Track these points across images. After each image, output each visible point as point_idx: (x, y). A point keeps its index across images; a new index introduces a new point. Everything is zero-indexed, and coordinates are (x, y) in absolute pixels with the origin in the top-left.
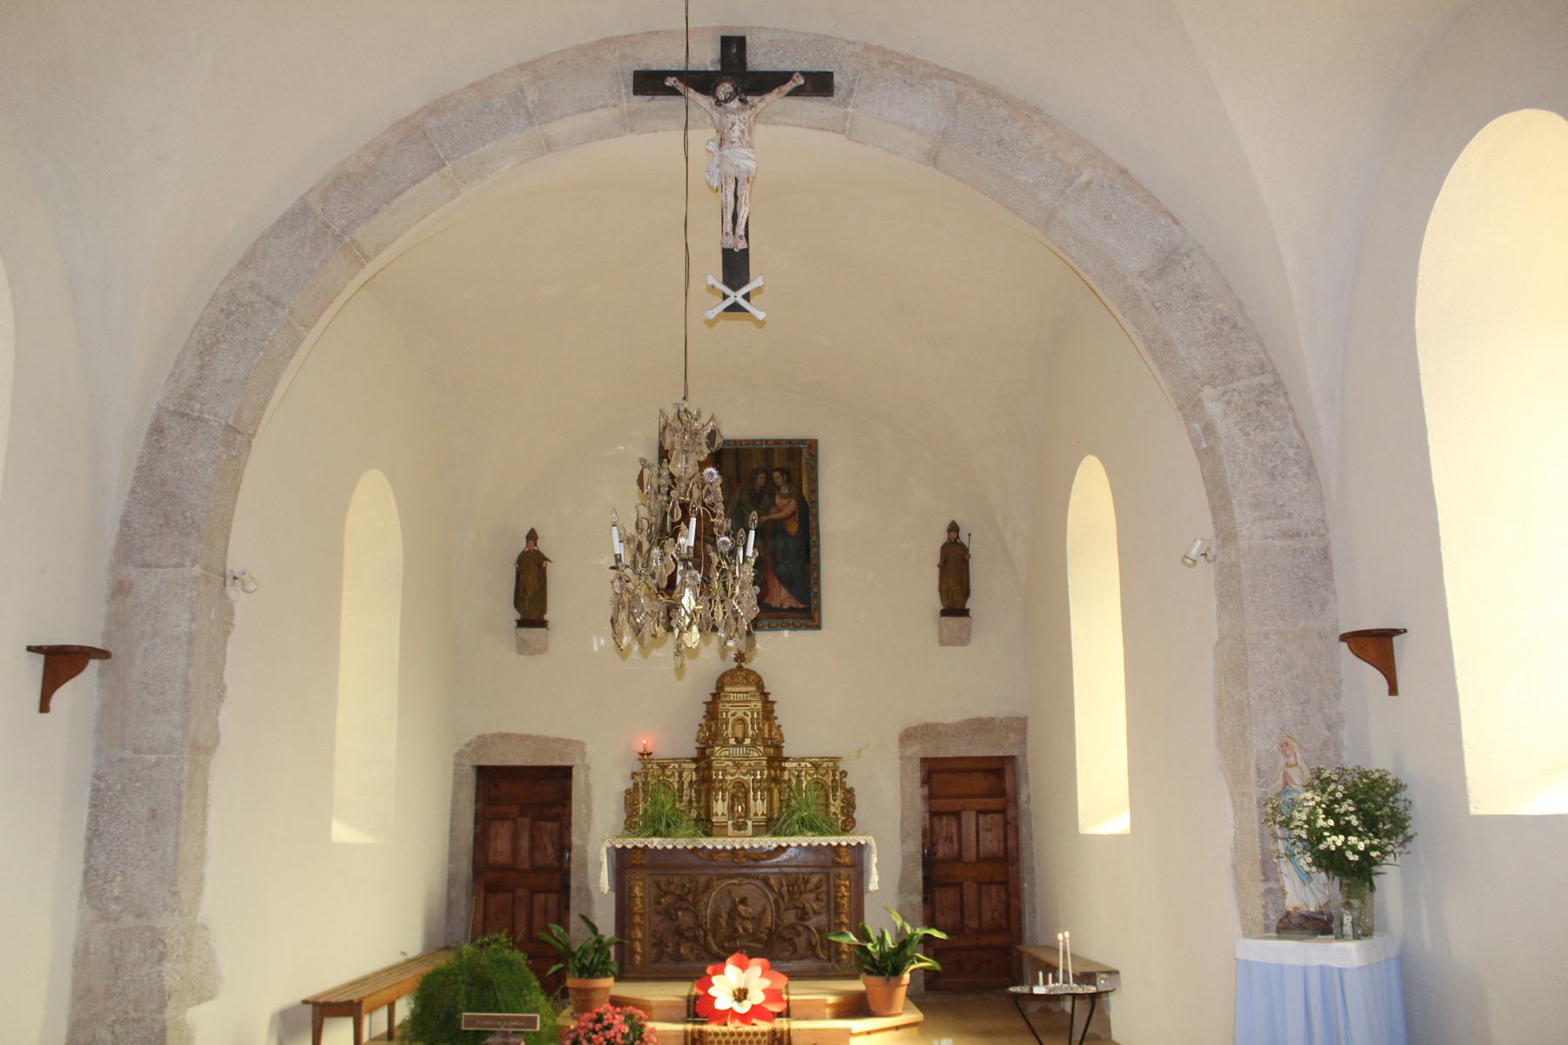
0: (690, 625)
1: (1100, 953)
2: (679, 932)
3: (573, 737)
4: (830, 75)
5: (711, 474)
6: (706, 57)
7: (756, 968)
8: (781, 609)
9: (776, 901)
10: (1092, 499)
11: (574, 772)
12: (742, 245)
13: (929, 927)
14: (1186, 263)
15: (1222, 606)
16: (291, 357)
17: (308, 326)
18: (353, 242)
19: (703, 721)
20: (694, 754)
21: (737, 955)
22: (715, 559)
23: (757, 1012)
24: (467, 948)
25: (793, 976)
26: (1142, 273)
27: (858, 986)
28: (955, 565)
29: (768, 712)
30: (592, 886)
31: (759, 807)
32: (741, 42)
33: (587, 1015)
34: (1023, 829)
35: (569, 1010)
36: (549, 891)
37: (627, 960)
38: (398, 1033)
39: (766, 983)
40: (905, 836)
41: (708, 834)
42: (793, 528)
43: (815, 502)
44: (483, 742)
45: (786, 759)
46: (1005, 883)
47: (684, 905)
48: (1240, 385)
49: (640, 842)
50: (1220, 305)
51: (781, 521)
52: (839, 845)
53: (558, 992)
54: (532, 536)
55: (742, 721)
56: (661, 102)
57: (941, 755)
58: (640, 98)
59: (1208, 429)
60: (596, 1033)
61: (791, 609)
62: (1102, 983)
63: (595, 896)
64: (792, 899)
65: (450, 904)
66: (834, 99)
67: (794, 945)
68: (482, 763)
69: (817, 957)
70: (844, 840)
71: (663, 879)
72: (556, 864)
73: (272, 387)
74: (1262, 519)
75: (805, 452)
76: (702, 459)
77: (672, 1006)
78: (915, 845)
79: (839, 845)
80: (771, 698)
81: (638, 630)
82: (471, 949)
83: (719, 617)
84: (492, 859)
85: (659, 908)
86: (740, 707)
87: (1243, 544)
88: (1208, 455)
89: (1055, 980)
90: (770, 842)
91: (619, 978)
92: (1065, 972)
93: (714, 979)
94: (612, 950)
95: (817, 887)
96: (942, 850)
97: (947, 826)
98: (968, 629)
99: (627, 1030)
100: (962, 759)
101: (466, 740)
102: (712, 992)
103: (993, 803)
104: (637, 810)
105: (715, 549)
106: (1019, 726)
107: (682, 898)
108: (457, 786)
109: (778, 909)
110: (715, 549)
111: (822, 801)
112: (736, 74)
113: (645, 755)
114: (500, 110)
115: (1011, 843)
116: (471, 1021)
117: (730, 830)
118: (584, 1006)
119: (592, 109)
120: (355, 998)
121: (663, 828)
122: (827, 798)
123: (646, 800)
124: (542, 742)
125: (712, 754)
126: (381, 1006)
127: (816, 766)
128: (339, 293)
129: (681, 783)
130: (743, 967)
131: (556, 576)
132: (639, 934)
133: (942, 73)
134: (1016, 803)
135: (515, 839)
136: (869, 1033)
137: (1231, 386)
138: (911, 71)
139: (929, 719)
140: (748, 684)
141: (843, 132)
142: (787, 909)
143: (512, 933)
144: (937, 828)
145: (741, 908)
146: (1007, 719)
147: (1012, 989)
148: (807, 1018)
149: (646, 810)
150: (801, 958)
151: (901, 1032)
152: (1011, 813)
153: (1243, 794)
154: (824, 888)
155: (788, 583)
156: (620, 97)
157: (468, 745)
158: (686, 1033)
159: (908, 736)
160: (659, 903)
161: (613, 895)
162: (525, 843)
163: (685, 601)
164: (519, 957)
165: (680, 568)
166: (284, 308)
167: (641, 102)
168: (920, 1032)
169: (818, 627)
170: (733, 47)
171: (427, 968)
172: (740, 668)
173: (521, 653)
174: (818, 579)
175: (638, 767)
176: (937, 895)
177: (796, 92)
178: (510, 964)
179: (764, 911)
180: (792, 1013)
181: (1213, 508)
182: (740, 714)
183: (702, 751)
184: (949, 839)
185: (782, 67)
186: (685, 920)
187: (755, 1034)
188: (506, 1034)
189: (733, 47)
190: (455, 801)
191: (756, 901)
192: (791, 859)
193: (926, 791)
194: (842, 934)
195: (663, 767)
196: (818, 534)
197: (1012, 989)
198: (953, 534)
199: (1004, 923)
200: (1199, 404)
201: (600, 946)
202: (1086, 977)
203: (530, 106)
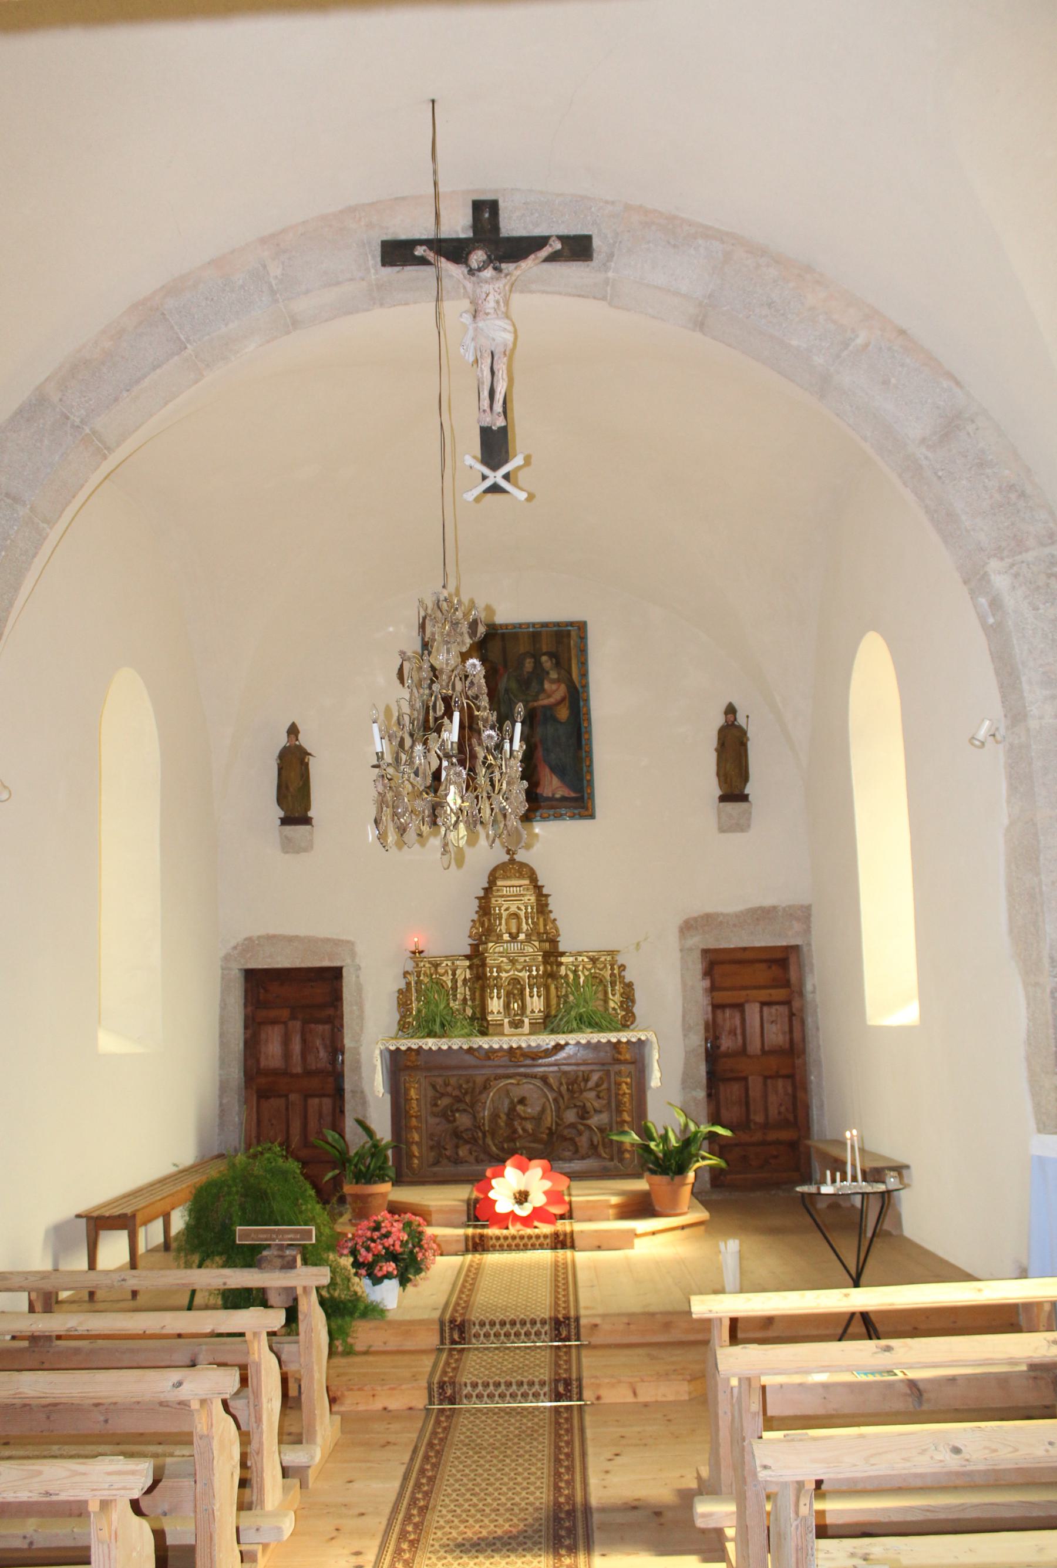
0: (456, 822)
1: (889, 1147)
2: (457, 1134)
3: (344, 938)
4: (588, 239)
5: (474, 665)
6: (458, 224)
7: (536, 1170)
8: (552, 799)
9: (555, 1100)
10: (874, 681)
12: (500, 422)
13: (713, 1124)
14: (970, 428)
15: (1013, 789)
16: (34, 556)
17: (51, 523)
18: (94, 432)
19: (475, 917)
21: (517, 1156)
22: (481, 753)
23: (539, 1214)
24: (241, 1158)
25: (573, 1176)
26: (923, 440)
27: (641, 1185)
28: (733, 747)
29: (542, 906)
31: (536, 1004)
33: (365, 1223)
34: (809, 1021)
35: (347, 1217)
36: (324, 1095)
37: (404, 1164)
38: (174, 1245)
39: (547, 1185)
40: (687, 1029)
41: (484, 1033)
42: (563, 714)
43: (586, 686)
44: (250, 945)
45: (563, 954)
46: (791, 1077)
47: (462, 1106)
48: (1030, 556)
49: (414, 1043)
50: (1007, 472)
51: (551, 708)
52: (619, 1042)
53: (334, 1200)
54: (293, 731)
55: (516, 916)
57: (724, 945)
58: (389, 270)
59: (996, 604)
60: (374, 1241)
61: (564, 799)
62: (892, 1182)
63: (370, 1098)
64: (573, 1098)
65: (223, 1111)
66: (594, 263)
67: (575, 1144)
69: (599, 1156)
70: (624, 1037)
71: (440, 1081)
72: (330, 1068)
73: (16, 589)
74: (1035, 1378)
75: (573, 634)
76: (464, 650)
77: (452, 1211)
78: (697, 1040)
79: (619, 1042)
80: (545, 891)
81: (402, 830)
82: (244, 1158)
83: (486, 813)
84: (263, 1063)
85: (435, 1109)
86: (513, 900)
87: (1033, 724)
88: (997, 635)
89: (844, 1179)
90: (547, 1041)
91: (398, 1182)
92: (854, 1166)
93: (494, 1182)
94: (390, 1153)
95: (598, 1085)
96: (726, 1043)
97: (730, 1019)
98: (748, 814)
99: (406, 1237)
100: (745, 949)
101: (233, 943)
102: (492, 1195)
103: (779, 994)
104: (410, 1010)
105: (480, 744)
106: (803, 915)
107: (458, 1100)
108: (225, 991)
109: (558, 1109)
110: (480, 744)
111: (601, 996)
112: (490, 240)
113: (417, 954)
115: (797, 1035)
116: (246, 1235)
117: (507, 1029)
118: (362, 1212)
119: (338, 283)
120: (128, 1211)
121: (437, 1028)
122: (606, 993)
123: (423, 1001)
124: (310, 943)
125: (486, 950)
126: (157, 1217)
127: (593, 960)
128: (82, 486)
129: (454, 981)
130: (523, 1169)
132: (416, 1137)
134: (801, 994)
135: (286, 1042)
136: (654, 1233)
137: (1018, 558)
138: (675, 231)
139: (709, 909)
140: (521, 876)
141: (604, 298)
142: (567, 1108)
143: (286, 1144)
144: (720, 1020)
145: (520, 1108)
146: (790, 907)
147: (799, 1189)
148: (590, 1220)
149: (419, 1011)
150: (583, 1158)
151: (687, 1231)
152: (796, 1004)
153: (1037, 984)
154: (605, 1086)
155: (559, 771)
156: (368, 270)
157: (235, 948)
158: (467, 1237)
159: (688, 927)
160: (436, 1105)
161: (388, 1097)
162: (296, 1047)
163: (450, 799)
164: (293, 1166)
165: (445, 763)
166: (24, 505)
167: (390, 273)
168: (706, 1231)
169: (592, 816)
170: (485, 212)
171: (198, 1179)
172: (512, 861)
173: (287, 852)
174: (590, 766)
175: (410, 966)
176: (722, 1088)
177: (553, 258)
178: (284, 1174)
179: (543, 1111)
180: (575, 1214)
181: (1001, 686)
182: (513, 909)
183: (475, 947)
184: (733, 1032)
185: (537, 232)
186: (465, 1123)
187: (538, 1237)
188: (281, 1247)
189: (485, 212)
190: (224, 1006)
191: (536, 1100)
192: (569, 1057)
193: (707, 983)
194: (624, 1133)
195: (436, 966)
196: (589, 720)
197: (799, 1189)
198: (731, 717)
199: (791, 1117)
200: (985, 577)
201: (376, 1150)
202: (874, 1175)
203: (274, 283)
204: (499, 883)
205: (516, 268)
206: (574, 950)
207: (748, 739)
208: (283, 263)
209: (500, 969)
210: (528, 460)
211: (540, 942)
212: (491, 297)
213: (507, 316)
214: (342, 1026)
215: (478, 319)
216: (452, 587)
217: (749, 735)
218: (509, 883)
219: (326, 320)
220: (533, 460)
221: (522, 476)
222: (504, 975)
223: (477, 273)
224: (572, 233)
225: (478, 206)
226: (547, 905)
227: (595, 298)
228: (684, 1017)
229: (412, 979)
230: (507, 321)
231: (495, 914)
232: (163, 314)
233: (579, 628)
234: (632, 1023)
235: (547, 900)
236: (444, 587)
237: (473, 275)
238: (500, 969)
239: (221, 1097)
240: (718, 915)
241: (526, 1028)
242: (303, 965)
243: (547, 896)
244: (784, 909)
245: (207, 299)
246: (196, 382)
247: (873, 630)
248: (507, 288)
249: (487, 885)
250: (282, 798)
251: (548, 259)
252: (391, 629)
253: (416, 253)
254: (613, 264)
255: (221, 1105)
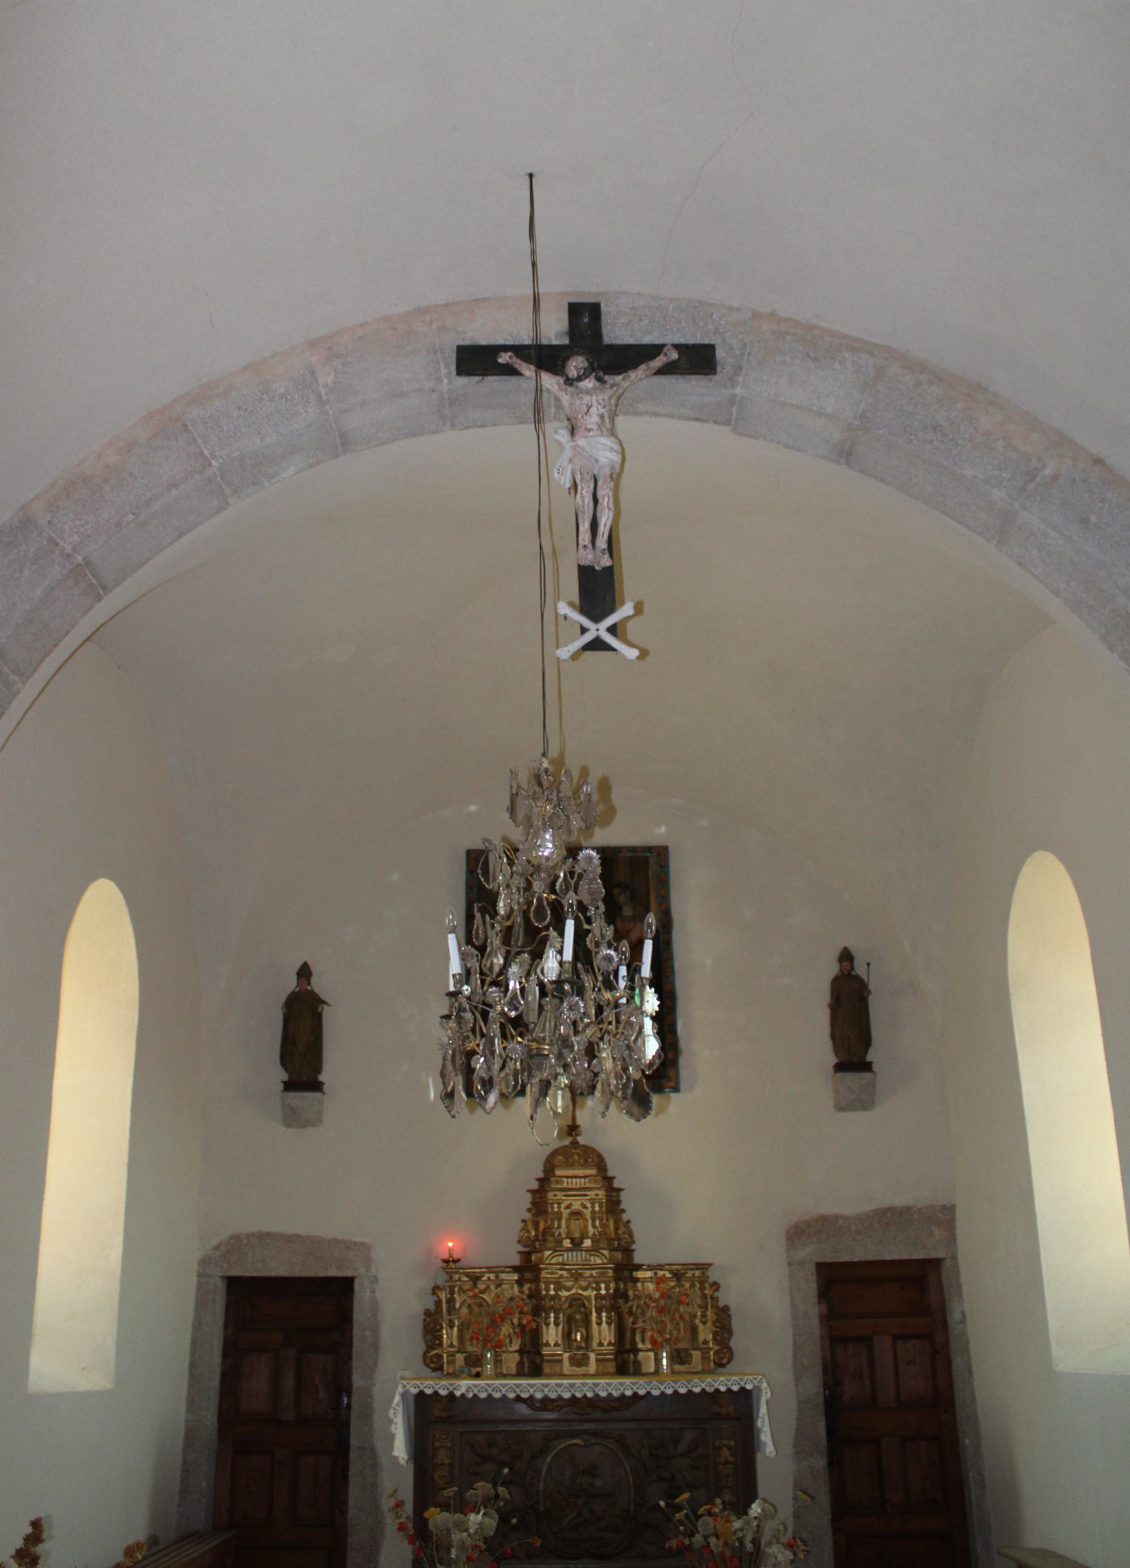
4: (711, 348)
6: (554, 329)
11: (356, 1287)
12: (606, 562)
19: (527, 1216)
20: (516, 1261)
28: (851, 1008)
29: (613, 1204)
30: (379, 1446)
32: (594, 310)
34: (958, 1361)
40: (799, 1371)
44: (236, 1245)
45: (639, 1267)
54: (304, 972)
55: (577, 1214)
56: (493, 382)
57: (844, 1258)
58: (464, 380)
68: (234, 1273)
70: (721, 1383)
75: (652, 863)
78: (813, 1385)
86: (576, 1194)
101: (215, 1242)
106: (944, 1217)
112: (591, 346)
113: (450, 1263)
114: (283, 396)
117: (566, 1367)
119: (403, 395)
124: (313, 1245)
127: (678, 1276)
131: (337, 1026)
133: (854, 345)
134: (945, 1325)
138: (817, 345)
140: (585, 1165)
141: (727, 423)
156: (439, 380)
157: (217, 1248)
159: (797, 1233)
161: (411, 1466)
162: (289, 1384)
170: (585, 317)
173: (288, 1126)
175: (441, 1280)
177: (667, 370)
182: (576, 1206)
183: (525, 1256)
185: (647, 340)
189: (585, 317)
190: (197, 1325)
195: (475, 1279)
203: (323, 393)
204: (558, 1172)
205: (623, 379)
206: (655, 1261)
207: (869, 992)
208: (335, 370)
209: (559, 1286)
210: (639, 609)
211: (611, 1250)
212: (593, 410)
213: (613, 433)
214: (350, 1358)
215: (577, 436)
216: (553, 752)
217: (871, 987)
218: (570, 1172)
219: (384, 443)
220: (646, 607)
221: (633, 630)
222: (564, 1293)
223: (575, 383)
224: (691, 342)
225: (575, 310)
226: (619, 1202)
227: (715, 422)
228: (795, 1354)
229: (443, 1296)
230: (613, 439)
231: (554, 1213)
232: (185, 425)
233: (659, 855)
234: (729, 1362)
235: (618, 1196)
236: (544, 755)
237: (571, 385)
238: (559, 1286)
239: (185, 1451)
240: (836, 1217)
241: (592, 1367)
242: (303, 1274)
243: (619, 1190)
244: (920, 1210)
245: (239, 408)
246: (219, 511)
247: (1047, 849)
248: (613, 401)
249: (541, 1175)
250: (286, 1057)
251: (661, 371)
252: (473, 808)
253: (500, 361)
254: (741, 379)
255: (185, 1463)
